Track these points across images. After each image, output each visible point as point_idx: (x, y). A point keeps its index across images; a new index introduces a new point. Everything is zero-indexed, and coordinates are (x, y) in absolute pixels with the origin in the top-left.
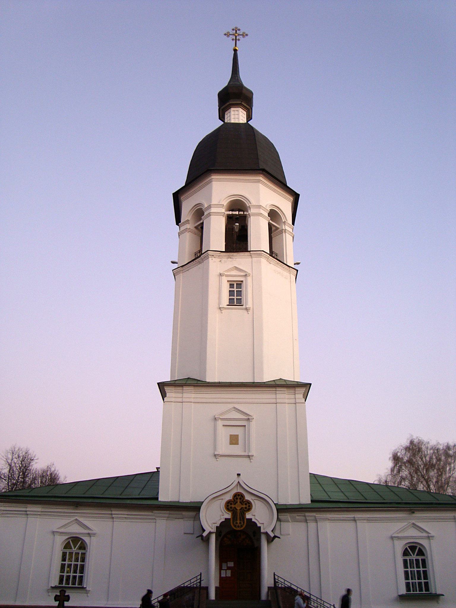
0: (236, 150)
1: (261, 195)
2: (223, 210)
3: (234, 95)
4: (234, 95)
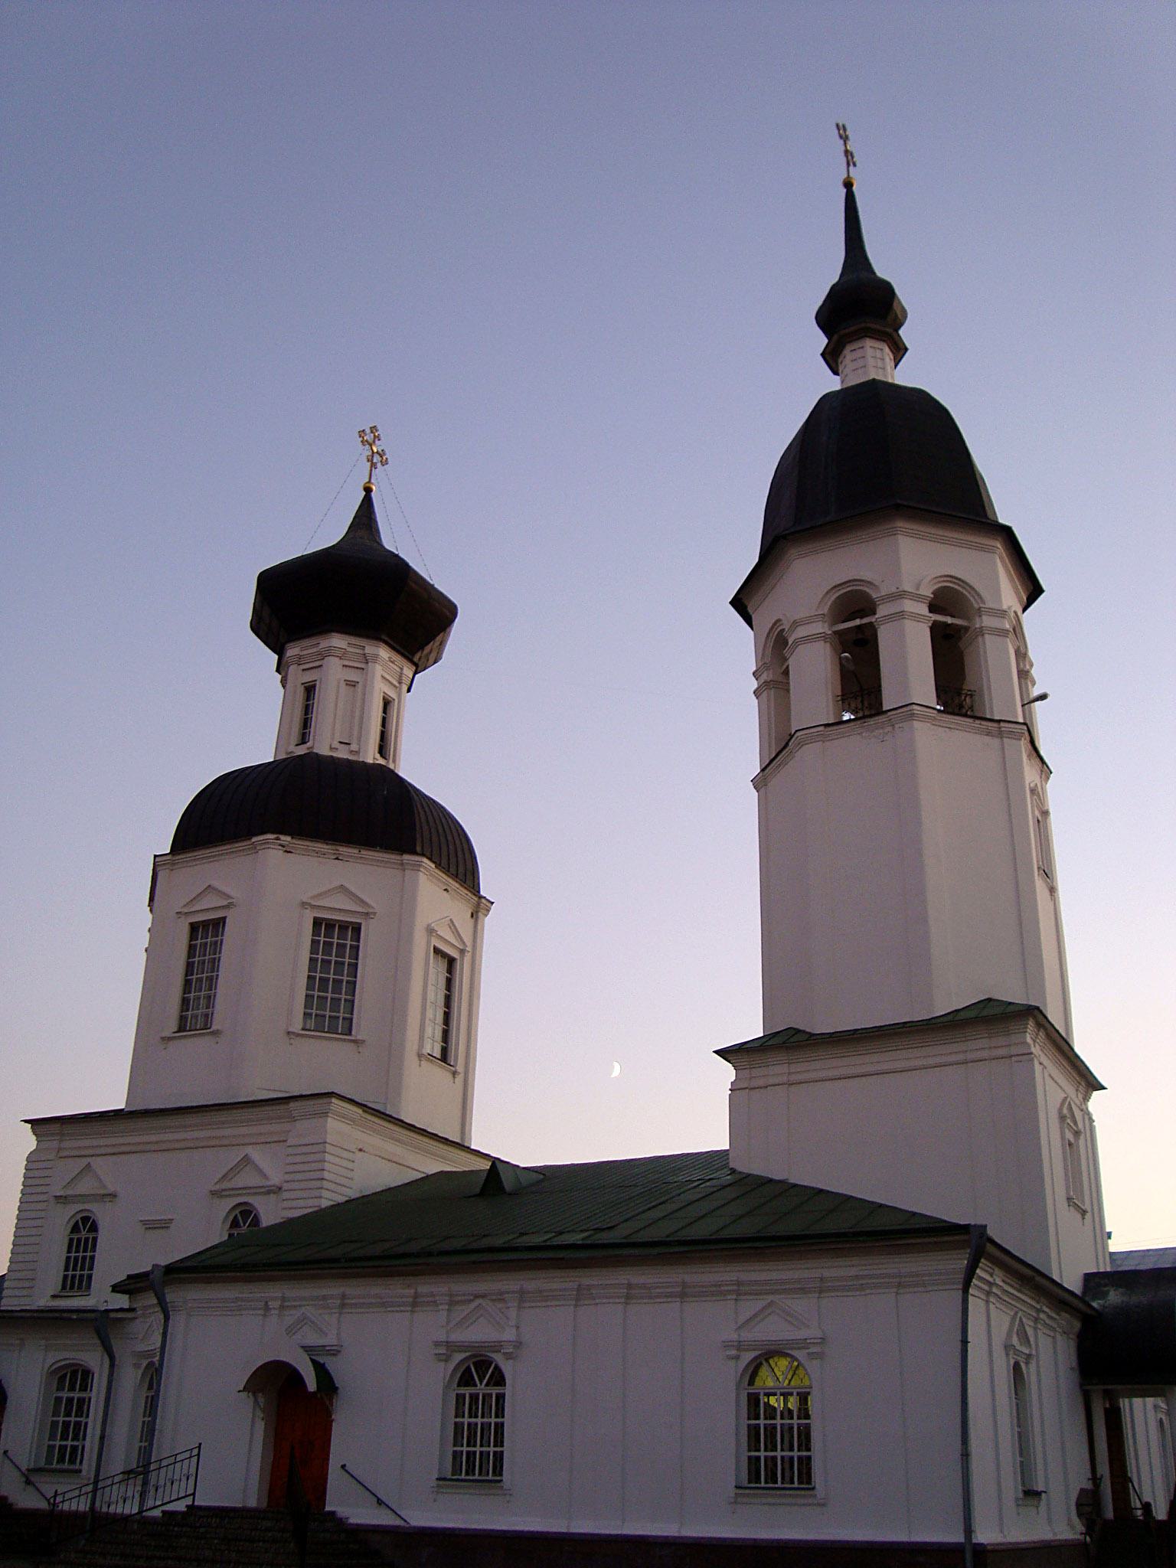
0: (876, 465)
3: (860, 308)
4: (860, 308)
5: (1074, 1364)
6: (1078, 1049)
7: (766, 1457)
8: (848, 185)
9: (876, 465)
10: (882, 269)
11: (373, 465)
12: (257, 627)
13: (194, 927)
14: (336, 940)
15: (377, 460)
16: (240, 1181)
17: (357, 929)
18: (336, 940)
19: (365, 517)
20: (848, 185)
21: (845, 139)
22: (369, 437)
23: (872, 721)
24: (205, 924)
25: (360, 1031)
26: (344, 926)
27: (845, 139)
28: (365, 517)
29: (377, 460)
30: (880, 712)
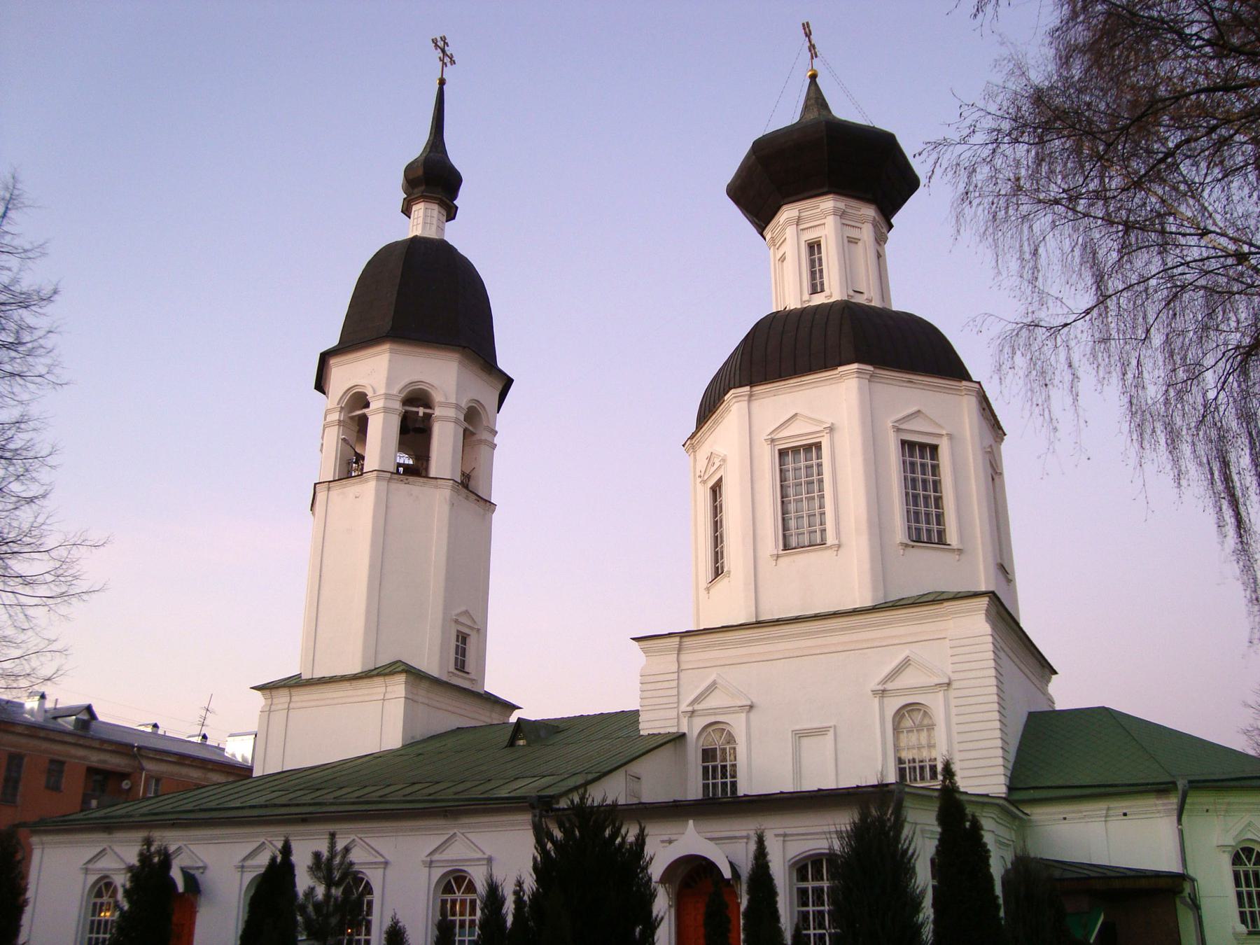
0: (424, 300)
1: (442, 374)
2: (397, 405)
3: (434, 180)
4: (434, 180)
5: (240, 932)
6: (1024, 625)
7: (813, 888)
8: (442, 82)
9: (424, 300)
10: (457, 156)
11: (444, 64)
12: (409, 169)
13: (783, 453)
14: (798, 461)
15: (447, 59)
16: (713, 702)
17: (934, 449)
18: (798, 461)
19: (815, 98)
20: (442, 82)
21: (808, 35)
22: (807, 30)
23: (411, 479)
24: (796, 450)
25: (952, 537)
26: (923, 446)
27: (808, 35)
28: (815, 98)
29: (447, 59)
30: (427, 477)
